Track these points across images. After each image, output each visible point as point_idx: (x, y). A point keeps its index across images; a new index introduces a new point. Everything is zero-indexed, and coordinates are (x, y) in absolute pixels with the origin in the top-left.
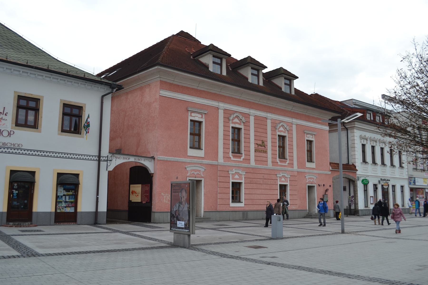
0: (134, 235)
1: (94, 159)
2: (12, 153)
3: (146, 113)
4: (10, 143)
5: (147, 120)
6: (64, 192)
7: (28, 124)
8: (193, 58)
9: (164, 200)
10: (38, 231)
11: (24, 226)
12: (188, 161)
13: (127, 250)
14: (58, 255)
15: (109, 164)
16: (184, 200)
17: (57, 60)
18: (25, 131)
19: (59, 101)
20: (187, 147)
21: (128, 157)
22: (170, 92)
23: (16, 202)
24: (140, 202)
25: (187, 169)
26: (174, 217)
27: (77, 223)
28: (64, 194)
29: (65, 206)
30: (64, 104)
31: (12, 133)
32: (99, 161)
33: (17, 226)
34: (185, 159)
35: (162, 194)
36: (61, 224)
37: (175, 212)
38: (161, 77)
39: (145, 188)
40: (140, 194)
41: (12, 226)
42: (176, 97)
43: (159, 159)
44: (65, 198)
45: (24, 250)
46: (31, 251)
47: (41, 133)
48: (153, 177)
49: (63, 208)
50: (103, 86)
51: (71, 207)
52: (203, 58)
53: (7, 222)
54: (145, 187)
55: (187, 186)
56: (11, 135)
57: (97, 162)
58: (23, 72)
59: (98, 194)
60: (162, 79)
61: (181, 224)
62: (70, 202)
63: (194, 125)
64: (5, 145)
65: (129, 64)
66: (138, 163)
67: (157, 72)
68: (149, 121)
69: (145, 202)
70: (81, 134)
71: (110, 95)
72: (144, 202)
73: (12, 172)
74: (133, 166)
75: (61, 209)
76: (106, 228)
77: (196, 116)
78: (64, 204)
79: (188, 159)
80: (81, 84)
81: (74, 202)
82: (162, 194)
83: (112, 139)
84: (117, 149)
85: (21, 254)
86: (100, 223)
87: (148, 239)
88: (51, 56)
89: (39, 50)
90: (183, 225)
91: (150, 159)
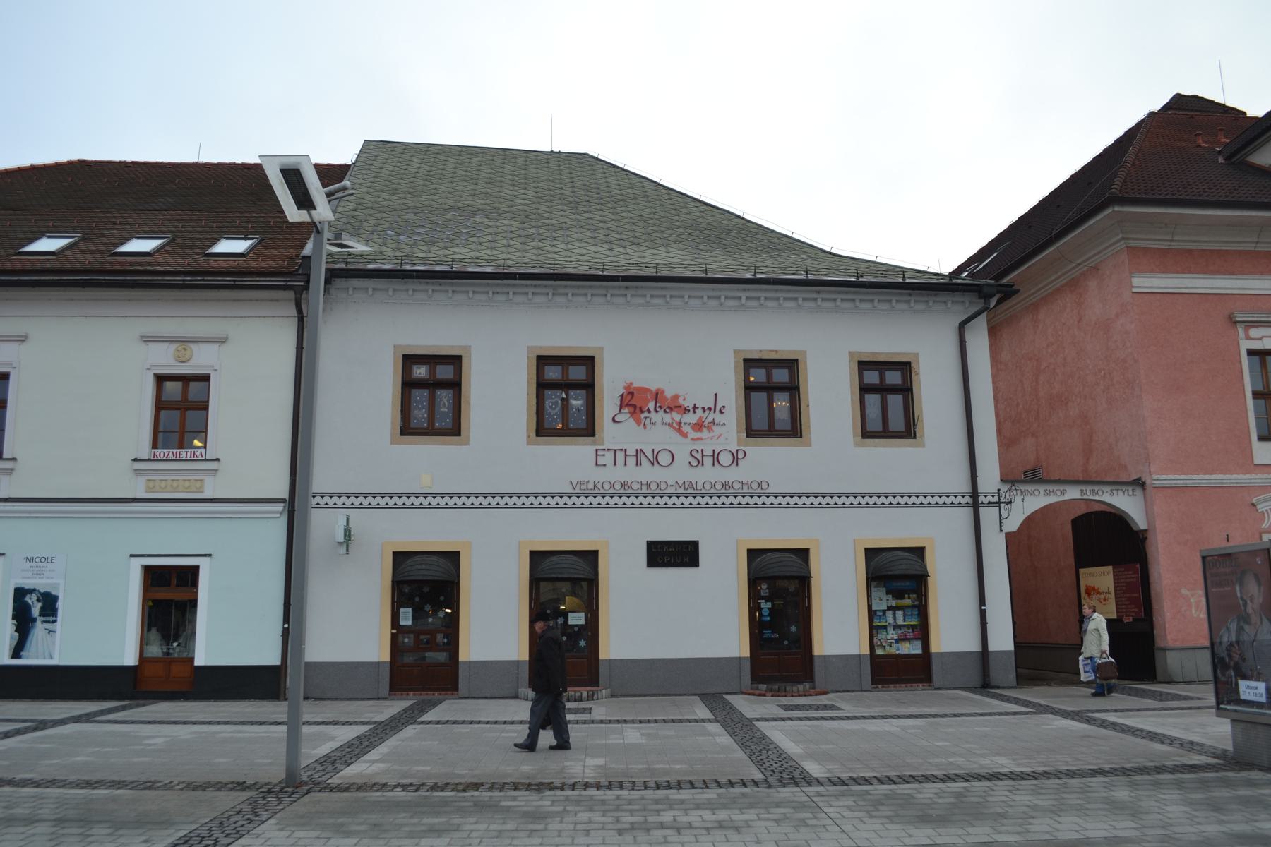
0: (1100, 722)
1: (960, 503)
2: (748, 506)
3: (1100, 353)
4: (638, 483)
5: (1105, 374)
6: (888, 600)
7: (777, 427)
8: (1225, 159)
9: (1194, 611)
10: (825, 707)
11: (794, 694)
12: (1260, 482)
13: (1071, 773)
14: (862, 782)
15: (1004, 514)
16: (1253, 609)
17: (830, 253)
18: (772, 446)
19: (392, 350)
20: (1250, 436)
21: (1061, 487)
22: (1163, 275)
23: (770, 632)
24: (1115, 619)
25: (1258, 507)
26: (1225, 667)
27: (932, 684)
28: (889, 605)
29: (896, 637)
30: (860, 363)
31: (741, 455)
32: (976, 507)
33: (777, 694)
34: (1248, 476)
35: (1184, 591)
36: (888, 687)
37: (1227, 650)
38: (1128, 239)
39: (1126, 575)
40: (1113, 595)
41: (764, 692)
42: (1186, 288)
43: (1159, 484)
44: (894, 615)
45: (776, 763)
46: (791, 766)
47: (810, 446)
48: (1148, 541)
49: (892, 642)
50: (958, 297)
51: (911, 641)
52: (1257, 151)
53: (752, 683)
54: (1126, 573)
55: (1259, 562)
56: (739, 461)
57: (969, 512)
58: (747, 298)
59: (982, 601)
60: (1132, 244)
61: (1252, 691)
62: (908, 626)
63: (1263, 364)
64: (626, 488)
65: (1030, 227)
66: (1093, 502)
67: (1113, 224)
68: (1110, 374)
69: (1131, 618)
70: (915, 437)
71: (982, 320)
72: (1126, 620)
73: (753, 554)
74: (1079, 513)
75: (885, 647)
76: (1015, 698)
77: (1265, 337)
78: (894, 632)
79: (1258, 476)
80: (897, 301)
81: (918, 627)
82: (1184, 591)
83: (1006, 442)
84: (1028, 468)
85: (763, 777)
86: (998, 685)
87: (1144, 738)
88: (816, 247)
89: (785, 239)
90: (1261, 695)
91: (1130, 489)
